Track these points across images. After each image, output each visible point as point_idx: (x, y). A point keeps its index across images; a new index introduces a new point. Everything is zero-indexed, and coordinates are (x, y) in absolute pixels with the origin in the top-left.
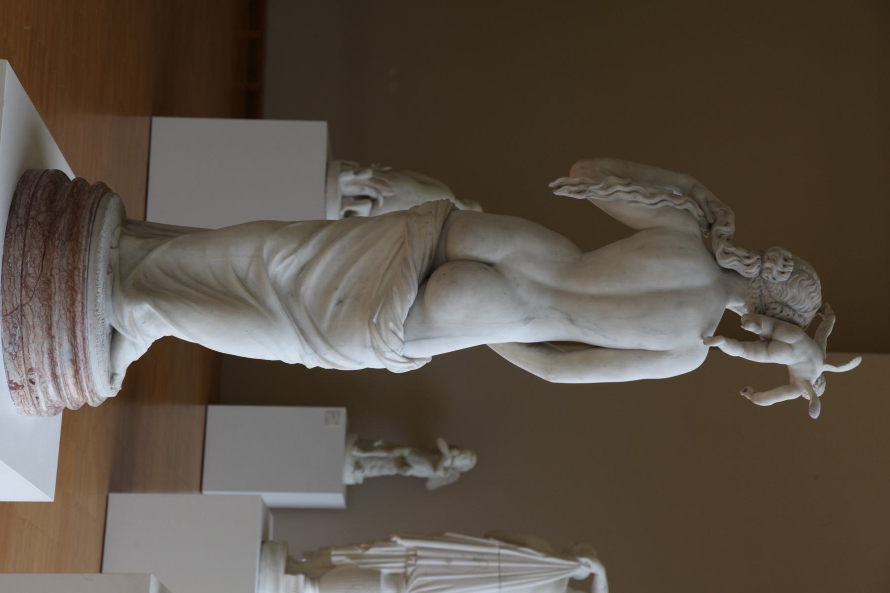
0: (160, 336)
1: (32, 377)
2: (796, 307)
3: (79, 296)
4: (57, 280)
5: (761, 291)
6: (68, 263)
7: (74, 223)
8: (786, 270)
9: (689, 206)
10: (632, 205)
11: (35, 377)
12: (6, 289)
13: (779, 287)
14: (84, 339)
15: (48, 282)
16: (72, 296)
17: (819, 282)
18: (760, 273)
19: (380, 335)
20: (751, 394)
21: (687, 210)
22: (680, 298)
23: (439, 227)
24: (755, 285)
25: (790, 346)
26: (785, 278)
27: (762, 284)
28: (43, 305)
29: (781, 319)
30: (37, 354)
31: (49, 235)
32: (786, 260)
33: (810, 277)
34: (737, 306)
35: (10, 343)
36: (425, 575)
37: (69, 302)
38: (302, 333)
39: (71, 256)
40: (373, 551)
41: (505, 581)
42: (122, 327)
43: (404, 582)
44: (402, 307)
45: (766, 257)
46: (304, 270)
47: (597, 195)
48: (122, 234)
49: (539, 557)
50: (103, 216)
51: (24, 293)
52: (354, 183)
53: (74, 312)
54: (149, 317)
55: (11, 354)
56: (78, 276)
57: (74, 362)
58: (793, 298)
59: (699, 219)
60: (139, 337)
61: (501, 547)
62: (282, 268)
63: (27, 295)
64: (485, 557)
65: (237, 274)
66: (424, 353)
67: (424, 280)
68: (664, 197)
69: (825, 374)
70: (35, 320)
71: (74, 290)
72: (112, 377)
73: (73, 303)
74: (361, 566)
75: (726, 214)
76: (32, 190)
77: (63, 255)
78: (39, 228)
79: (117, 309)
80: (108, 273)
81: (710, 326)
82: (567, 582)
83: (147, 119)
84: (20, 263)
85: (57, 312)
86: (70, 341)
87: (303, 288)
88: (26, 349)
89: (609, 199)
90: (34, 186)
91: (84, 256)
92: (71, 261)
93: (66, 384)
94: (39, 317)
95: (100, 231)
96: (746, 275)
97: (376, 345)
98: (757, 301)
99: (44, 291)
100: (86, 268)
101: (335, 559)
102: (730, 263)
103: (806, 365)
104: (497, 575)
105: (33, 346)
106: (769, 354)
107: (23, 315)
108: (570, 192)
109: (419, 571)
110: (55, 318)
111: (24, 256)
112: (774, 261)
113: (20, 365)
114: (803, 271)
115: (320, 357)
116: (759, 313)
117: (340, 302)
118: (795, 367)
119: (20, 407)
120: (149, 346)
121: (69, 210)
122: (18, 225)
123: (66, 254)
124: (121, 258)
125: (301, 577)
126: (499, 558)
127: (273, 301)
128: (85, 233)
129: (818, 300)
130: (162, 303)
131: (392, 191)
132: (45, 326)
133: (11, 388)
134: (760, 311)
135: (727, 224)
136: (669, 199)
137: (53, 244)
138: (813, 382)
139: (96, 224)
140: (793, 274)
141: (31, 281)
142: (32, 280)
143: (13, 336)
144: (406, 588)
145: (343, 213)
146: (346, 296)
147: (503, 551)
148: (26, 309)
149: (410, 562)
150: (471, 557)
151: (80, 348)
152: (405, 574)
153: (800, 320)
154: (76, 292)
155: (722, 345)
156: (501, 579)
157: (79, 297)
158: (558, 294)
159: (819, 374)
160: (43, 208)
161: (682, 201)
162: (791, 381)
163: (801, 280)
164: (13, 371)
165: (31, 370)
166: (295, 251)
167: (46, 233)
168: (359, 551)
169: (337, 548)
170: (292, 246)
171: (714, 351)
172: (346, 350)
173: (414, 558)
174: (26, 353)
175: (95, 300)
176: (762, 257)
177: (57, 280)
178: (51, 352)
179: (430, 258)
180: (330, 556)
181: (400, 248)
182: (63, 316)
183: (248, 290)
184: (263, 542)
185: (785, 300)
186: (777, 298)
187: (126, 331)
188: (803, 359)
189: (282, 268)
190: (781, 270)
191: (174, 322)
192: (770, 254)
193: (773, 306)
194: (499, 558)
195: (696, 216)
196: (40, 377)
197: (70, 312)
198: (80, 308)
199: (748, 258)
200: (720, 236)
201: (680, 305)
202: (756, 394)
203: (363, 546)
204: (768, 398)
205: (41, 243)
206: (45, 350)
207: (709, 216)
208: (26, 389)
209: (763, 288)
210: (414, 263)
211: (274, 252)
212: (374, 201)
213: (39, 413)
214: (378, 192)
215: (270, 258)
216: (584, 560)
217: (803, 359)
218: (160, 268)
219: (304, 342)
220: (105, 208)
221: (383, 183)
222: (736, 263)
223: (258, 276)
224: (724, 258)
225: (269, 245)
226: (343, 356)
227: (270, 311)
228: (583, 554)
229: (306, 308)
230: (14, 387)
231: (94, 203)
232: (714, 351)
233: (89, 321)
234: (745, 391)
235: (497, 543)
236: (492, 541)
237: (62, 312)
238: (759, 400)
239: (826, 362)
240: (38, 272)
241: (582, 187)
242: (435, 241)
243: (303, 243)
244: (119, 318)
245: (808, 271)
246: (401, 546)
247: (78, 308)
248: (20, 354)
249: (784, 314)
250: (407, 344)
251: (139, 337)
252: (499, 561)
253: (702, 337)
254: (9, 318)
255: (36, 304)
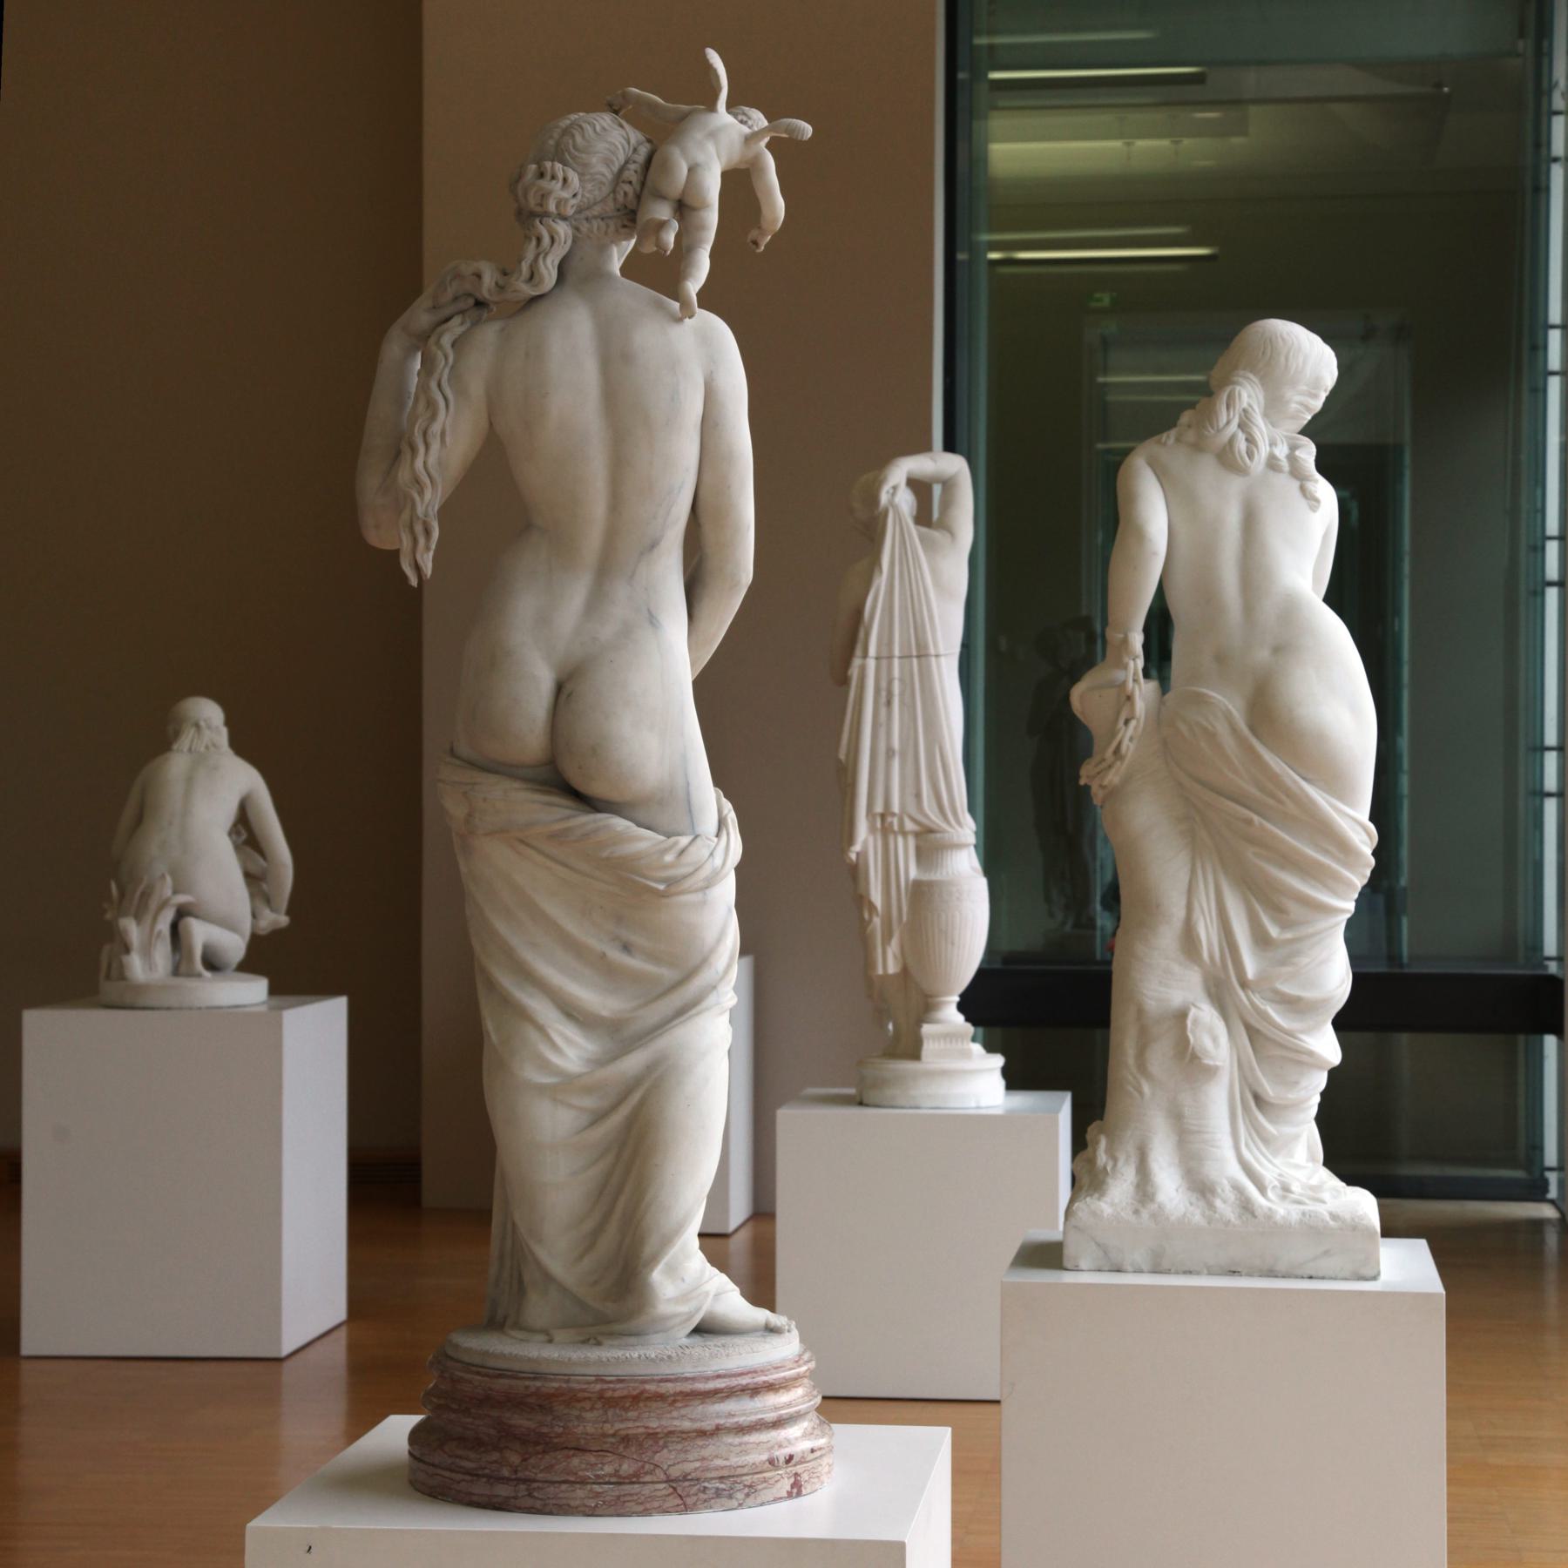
0: (700, 1255)
1: (782, 1460)
2: (622, 158)
3: (647, 1387)
4: (622, 1426)
5: (595, 217)
6: (592, 1409)
7: (518, 1402)
8: (560, 175)
9: (447, 340)
10: (448, 439)
11: (781, 1454)
12: (641, 1508)
13: (589, 186)
14: (719, 1376)
15: (626, 1440)
16: (648, 1399)
17: (573, 117)
18: (565, 219)
19: (685, 877)
20: (764, 235)
21: (453, 345)
22: (616, 360)
23: (492, 778)
24: (585, 227)
25: (692, 170)
26: (573, 177)
27: (582, 216)
28: (665, 1446)
29: (643, 184)
30: (746, 1452)
31: (542, 1443)
32: (542, 175)
33: (566, 132)
34: (616, 259)
35: (730, 1497)
36: (918, 795)
37: (660, 1404)
38: (683, 1011)
39: (579, 1405)
40: (876, 897)
41: (926, 647)
42: (690, 1316)
43: (932, 836)
44: (644, 841)
45: (538, 209)
46: (572, 1012)
47: (429, 502)
48: (518, 1326)
49: (881, 582)
50: (502, 1356)
51: (648, 1478)
52: (147, 953)
53: (676, 1394)
54: (672, 1270)
55: (748, 1495)
56: (614, 1390)
57: (754, 1391)
58: (607, 162)
59: (468, 324)
60: (707, 1287)
61: (865, 655)
62: (571, 1050)
63: (651, 1473)
64: (884, 684)
65: (585, 1128)
66: (709, 802)
67: (587, 802)
68: (433, 385)
69: (730, 106)
70: (691, 1457)
71: (639, 1397)
72: (771, 1330)
73: (661, 1397)
74: (905, 918)
75: (458, 276)
76: (459, 1477)
77: (578, 1418)
78: (532, 1461)
79: (661, 1325)
80: (599, 1344)
81: (660, 306)
82: (924, 530)
83: (25, 1365)
84: (597, 1488)
85: (676, 1423)
86: (723, 1399)
87: (605, 1013)
88: (739, 1471)
89: (438, 480)
90: (453, 1475)
91: (578, 1382)
92: (587, 1405)
93: (789, 1405)
94: (686, 1452)
95: (529, 1360)
96: (569, 242)
97: (701, 884)
98: (612, 224)
99: (641, 1445)
100: (599, 1379)
101: (892, 968)
102: (549, 272)
103: (722, 140)
104: (915, 661)
105: (734, 1460)
106: (705, 205)
107: (685, 1478)
108: (428, 548)
109: (912, 810)
110: (687, 1425)
111: (583, 1482)
112: (544, 196)
113: (765, 1480)
114: (558, 144)
115: (722, 979)
116: (634, 221)
117: (626, 948)
118: (724, 160)
119: (824, 1478)
120: (716, 1271)
121: (495, 1413)
122: (530, 1495)
123: (576, 1413)
124: (564, 1326)
125: (926, 1029)
126: (885, 658)
127: (633, 1063)
128: (538, 1384)
129: (605, 120)
130: (648, 1250)
131: (163, 876)
132: (700, 1442)
133: (799, 1494)
134: (629, 217)
135: (479, 276)
136: (436, 376)
137: (559, 1436)
138: (746, 130)
139: (517, 1366)
140: (565, 163)
141: (627, 1468)
142: (625, 1467)
143: (718, 1493)
144: (943, 831)
145: (207, 974)
146: (615, 938)
147: (872, 651)
148: (675, 1472)
149: (896, 828)
150: (883, 711)
151: (734, 1382)
152: (917, 835)
153: (644, 150)
154: (642, 1392)
155: (694, 285)
156: (923, 655)
157: (651, 1387)
158: (607, 569)
159: (730, 119)
160: (495, 1456)
161: (440, 353)
162: (743, 167)
163: (575, 147)
164: (774, 1490)
165: (771, 1462)
166: (541, 1029)
167: (539, 1448)
168: (877, 921)
169: (868, 962)
170: (533, 1035)
171: (708, 299)
172: (710, 936)
173: (889, 819)
174: (745, 1471)
175: (652, 1360)
176: (533, 215)
177: (622, 1426)
178: (742, 1430)
179: (549, 793)
180: (886, 976)
181: (528, 845)
182: (683, 1412)
183: (615, 1107)
184: (861, 1104)
185: (610, 176)
186: (606, 190)
187: (698, 1310)
188: (711, 147)
189: (571, 1050)
190: (560, 184)
191: (678, 1230)
192: (532, 202)
193: (620, 198)
194: (885, 658)
195: (463, 329)
196: (780, 1446)
197: (675, 1401)
198: (669, 1385)
199: (539, 240)
200: (501, 288)
201: (628, 357)
202: (764, 225)
203: (866, 916)
204: (773, 205)
205: (559, 1455)
206: (737, 1440)
207: (462, 305)
208: (799, 1469)
209: (588, 213)
210: (562, 819)
211: (545, 1066)
212: (182, 913)
213: (831, 1449)
214: (164, 904)
215: (558, 1072)
216: (884, 498)
217: (711, 147)
218: (580, 1258)
219: (699, 1008)
220: (486, 1353)
221: (146, 895)
222: (549, 261)
223: (588, 1090)
224: (541, 281)
225: (531, 1074)
226: (719, 940)
227: (651, 1068)
228: (875, 500)
229: (646, 1004)
230: (797, 1489)
231: (478, 1373)
232: (708, 299)
233: (688, 1370)
234: (756, 243)
235: (857, 662)
236: (854, 672)
237: (675, 1414)
238: (775, 220)
239: (711, 107)
240: (611, 1457)
241: (419, 529)
242: (516, 785)
243: (524, 1015)
244: (678, 1320)
245: (556, 135)
246: (865, 843)
247: (669, 1388)
248: (748, 1480)
249: (634, 178)
250: (699, 830)
251: (707, 1287)
252: (890, 657)
253: (680, 320)
254: (689, 1501)
255: (665, 1457)
